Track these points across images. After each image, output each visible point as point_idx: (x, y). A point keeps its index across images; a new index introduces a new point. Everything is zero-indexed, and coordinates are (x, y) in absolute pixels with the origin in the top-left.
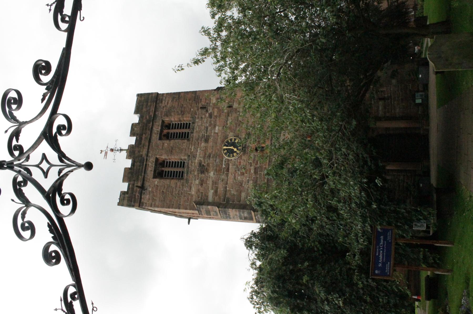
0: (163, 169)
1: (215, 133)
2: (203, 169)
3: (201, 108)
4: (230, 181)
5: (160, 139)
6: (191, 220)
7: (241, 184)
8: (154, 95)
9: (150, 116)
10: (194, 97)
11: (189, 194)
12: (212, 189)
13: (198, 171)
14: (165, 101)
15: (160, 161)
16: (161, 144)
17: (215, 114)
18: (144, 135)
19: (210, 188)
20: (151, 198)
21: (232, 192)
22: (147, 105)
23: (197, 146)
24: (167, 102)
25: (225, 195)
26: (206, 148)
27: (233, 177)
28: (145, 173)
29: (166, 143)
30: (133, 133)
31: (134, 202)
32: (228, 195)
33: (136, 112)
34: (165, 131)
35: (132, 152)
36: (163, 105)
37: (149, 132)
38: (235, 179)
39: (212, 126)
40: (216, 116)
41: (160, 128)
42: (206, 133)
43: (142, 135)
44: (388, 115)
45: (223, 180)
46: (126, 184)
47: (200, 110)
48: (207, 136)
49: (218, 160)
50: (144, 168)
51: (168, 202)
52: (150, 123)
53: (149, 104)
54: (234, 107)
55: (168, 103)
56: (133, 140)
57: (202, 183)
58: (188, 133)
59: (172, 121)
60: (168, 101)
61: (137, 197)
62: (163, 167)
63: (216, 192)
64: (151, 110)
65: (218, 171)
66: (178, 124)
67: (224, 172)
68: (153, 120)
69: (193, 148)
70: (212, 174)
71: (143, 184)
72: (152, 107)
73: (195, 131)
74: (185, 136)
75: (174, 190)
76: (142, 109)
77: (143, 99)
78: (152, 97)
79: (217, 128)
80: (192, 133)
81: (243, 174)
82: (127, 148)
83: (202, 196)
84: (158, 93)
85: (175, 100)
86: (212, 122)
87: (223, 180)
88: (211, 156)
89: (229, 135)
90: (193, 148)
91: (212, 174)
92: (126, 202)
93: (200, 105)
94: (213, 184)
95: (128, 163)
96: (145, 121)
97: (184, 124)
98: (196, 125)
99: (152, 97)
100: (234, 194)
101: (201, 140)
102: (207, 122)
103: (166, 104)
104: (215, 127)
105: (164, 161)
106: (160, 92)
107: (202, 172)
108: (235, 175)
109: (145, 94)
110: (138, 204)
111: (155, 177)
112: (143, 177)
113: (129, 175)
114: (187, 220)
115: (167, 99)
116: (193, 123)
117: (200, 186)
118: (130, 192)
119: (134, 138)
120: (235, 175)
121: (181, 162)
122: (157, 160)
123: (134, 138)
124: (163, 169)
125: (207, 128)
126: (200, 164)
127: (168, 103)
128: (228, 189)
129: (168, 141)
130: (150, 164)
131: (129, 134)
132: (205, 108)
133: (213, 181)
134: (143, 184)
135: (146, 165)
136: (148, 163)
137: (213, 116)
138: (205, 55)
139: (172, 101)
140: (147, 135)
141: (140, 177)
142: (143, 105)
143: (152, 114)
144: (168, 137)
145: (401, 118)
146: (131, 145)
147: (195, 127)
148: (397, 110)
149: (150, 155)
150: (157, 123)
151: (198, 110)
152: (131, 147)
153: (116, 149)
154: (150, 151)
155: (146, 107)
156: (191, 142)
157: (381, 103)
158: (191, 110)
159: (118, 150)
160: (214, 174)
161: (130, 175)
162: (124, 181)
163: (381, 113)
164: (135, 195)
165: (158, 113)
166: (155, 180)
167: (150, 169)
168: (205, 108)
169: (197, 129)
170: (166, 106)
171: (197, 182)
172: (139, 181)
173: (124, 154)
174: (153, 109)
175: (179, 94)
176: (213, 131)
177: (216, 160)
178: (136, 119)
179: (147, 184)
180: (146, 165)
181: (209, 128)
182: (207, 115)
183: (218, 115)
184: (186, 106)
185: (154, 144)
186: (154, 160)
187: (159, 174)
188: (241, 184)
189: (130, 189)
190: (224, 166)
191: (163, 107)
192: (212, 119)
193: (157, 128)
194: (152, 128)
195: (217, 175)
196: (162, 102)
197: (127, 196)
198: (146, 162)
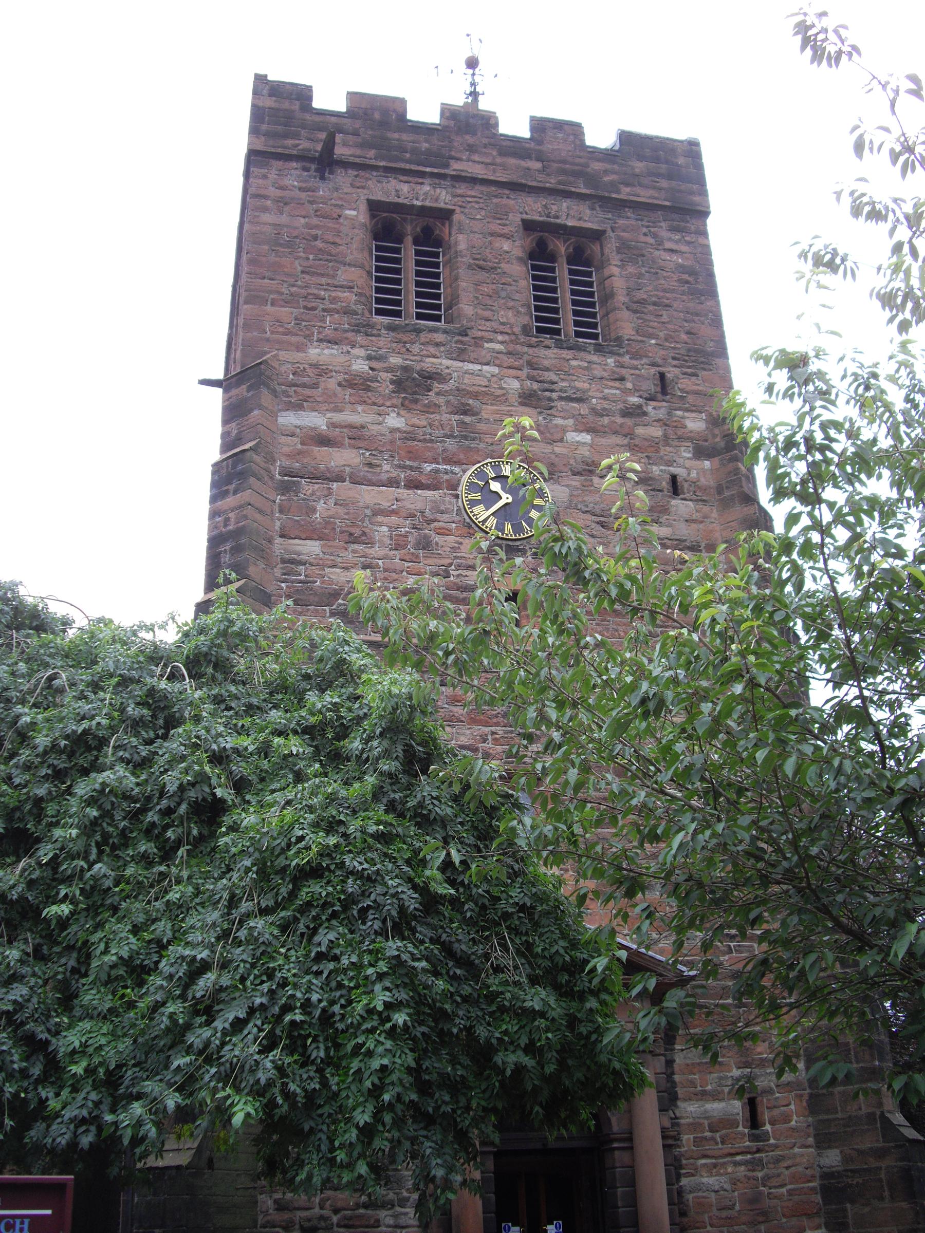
0: (409, 240)
1: (564, 430)
2: (413, 386)
3: (662, 376)
4: (369, 496)
5: (529, 226)
6: (220, 391)
7: (364, 539)
8: (696, 199)
9: (614, 186)
10: (705, 353)
11: (309, 337)
12: (333, 425)
13: (406, 369)
14: (677, 242)
15: (443, 231)
16: (506, 230)
17: (640, 431)
18: (538, 165)
19: (338, 417)
20: (286, 193)
21: (320, 506)
22: (659, 175)
23: (511, 361)
24: (674, 247)
25: (313, 477)
26: (501, 399)
27: (385, 504)
28: (387, 169)
29: (513, 248)
30: (540, 126)
31: (267, 134)
32: (307, 488)
33: (626, 138)
34: (561, 248)
35: (468, 125)
36: (664, 234)
37: (552, 182)
38: (375, 514)
39: (591, 418)
40: (630, 434)
41: (570, 223)
42: (561, 398)
43: (538, 159)
44: (687, 1138)
45: (370, 465)
46: (341, 106)
47: (653, 370)
48: (550, 399)
49: (451, 444)
50: (408, 166)
51: (273, 258)
52: (586, 187)
53: (664, 183)
54: (674, 502)
55: (672, 251)
56: (514, 125)
57: (360, 386)
58: (557, 332)
59: (600, 268)
60: (681, 253)
61: (290, 142)
62: (416, 242)
63: (324, 441)
64: (638, 190)
65: (409, 446)
66: (591, 295)
67: (403, 467)
68: (601, 199)
69: (498, 347)
70: (394, 421)
71: (345, 165)
72: (651, 192)
73: (567, 354)
74: (546, 323)
75: (324, 280)
76: (641, 158)
77: (681, 161)
78: (692, 193)
79: (586, 438)
80: (560, 345)
81: (399, 544)
82: (484, 105)
83: (304, 386)
84: (705, 214)
85: (686, 277)
86: (606, 420)
87: (370, 465)
88: (468, 419)
89: (556, 487)
90: (498, 347)
91: (394, 421)
92: (269, 102)
93: (671, 373)
94: (351, 426)
95: (424, 111)
96: (596, 166)
97: (594, 315)
98: (595, 358)
99: (692, 193)
100: (314, 510)
101: (531, 378)
102: (605, 398)
103: (668, 245)
104: (588, 431)
105: (438, 243)
106: (712, 223)
107: (399, 385)
108: (394, 512)
109: (699, 167)
110: (259, 147)
111: (374, 207)
112: (373, 162)
113: (377, 117)
114: (219, 375)
115: (684, 248)
116: (599, 349)
117: (340, 378)
118: (308, 117)
119: (526, 133)
120: (394, 512)
121: (438, 307)
122: (445, 215)
123: (526, 133)
124: (409, 240)
125: (579, 400)
126: (430, 377)
127: (672, 251)
128: (335, 485)
129: (518, 252)
130: (427, 188)
131: (539, 114)
132: (664, 391)
133: (363, 427)
134: (345, 165)
135: (422, 174)
136: (427, 181)
137: (629, 421)
138: (441, 1009)
139: (681, 266)
140: (541, 177)
141: (372, 153)
142: (657, 160)
143: (625, 193)
144: (540, 257)
145: (677, 1198)
146: (497, 118)
147: (582, 354)
148: (708, 1180)
149: (462, 189)
150: (588, 211)
151: (654, 365)
152: (488, 122)
153: (477, 79)
154: (478, 187)
155: (651, 174)
156: (522, 339)
157: (737, 1106)
158: (651, 336)
159: (473, 84)
160: (393, 430)
161: (377, 116)
162: (353, 97)
163: (689, 1109)
164: (296, 136)
165: (628, 220)
166: (363, 207)
167: (405, 188)
168: (664, 391)
169: (574, 363)
170: (660, 243)
171: (360, 366)
172: (358, 152)
173: (459, 99)
174: (645, 195)
175: (711, 292)
176: (570, 422)
177: (451, 436)
178: (600, 136)
179: (343, 179)
180: (422, 174)
181: (584, 409)
182: (634, 400)
183: (637, 441)
184: (665, 318)
185: (505, 201)
186: (442, 205)
187: (387, 225)
188: (364, 539)
189: (318, 119)
190: (428, 467)
191: (655, 236)
192: (619, 420)
193: (572, 214)
194: (568, 195)
195: (392, 442)
196: (673, 229)
197: (296, 106)
198: (432, 175)
